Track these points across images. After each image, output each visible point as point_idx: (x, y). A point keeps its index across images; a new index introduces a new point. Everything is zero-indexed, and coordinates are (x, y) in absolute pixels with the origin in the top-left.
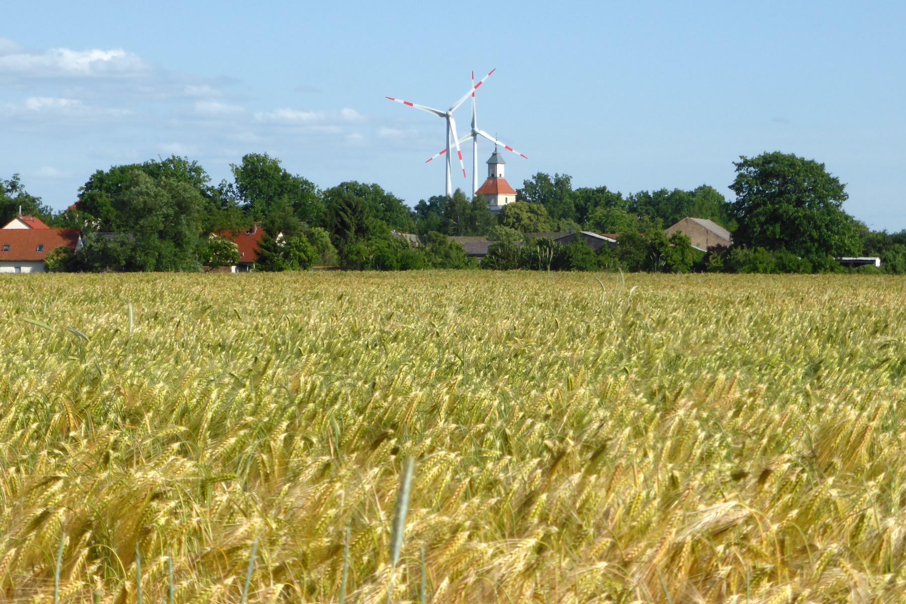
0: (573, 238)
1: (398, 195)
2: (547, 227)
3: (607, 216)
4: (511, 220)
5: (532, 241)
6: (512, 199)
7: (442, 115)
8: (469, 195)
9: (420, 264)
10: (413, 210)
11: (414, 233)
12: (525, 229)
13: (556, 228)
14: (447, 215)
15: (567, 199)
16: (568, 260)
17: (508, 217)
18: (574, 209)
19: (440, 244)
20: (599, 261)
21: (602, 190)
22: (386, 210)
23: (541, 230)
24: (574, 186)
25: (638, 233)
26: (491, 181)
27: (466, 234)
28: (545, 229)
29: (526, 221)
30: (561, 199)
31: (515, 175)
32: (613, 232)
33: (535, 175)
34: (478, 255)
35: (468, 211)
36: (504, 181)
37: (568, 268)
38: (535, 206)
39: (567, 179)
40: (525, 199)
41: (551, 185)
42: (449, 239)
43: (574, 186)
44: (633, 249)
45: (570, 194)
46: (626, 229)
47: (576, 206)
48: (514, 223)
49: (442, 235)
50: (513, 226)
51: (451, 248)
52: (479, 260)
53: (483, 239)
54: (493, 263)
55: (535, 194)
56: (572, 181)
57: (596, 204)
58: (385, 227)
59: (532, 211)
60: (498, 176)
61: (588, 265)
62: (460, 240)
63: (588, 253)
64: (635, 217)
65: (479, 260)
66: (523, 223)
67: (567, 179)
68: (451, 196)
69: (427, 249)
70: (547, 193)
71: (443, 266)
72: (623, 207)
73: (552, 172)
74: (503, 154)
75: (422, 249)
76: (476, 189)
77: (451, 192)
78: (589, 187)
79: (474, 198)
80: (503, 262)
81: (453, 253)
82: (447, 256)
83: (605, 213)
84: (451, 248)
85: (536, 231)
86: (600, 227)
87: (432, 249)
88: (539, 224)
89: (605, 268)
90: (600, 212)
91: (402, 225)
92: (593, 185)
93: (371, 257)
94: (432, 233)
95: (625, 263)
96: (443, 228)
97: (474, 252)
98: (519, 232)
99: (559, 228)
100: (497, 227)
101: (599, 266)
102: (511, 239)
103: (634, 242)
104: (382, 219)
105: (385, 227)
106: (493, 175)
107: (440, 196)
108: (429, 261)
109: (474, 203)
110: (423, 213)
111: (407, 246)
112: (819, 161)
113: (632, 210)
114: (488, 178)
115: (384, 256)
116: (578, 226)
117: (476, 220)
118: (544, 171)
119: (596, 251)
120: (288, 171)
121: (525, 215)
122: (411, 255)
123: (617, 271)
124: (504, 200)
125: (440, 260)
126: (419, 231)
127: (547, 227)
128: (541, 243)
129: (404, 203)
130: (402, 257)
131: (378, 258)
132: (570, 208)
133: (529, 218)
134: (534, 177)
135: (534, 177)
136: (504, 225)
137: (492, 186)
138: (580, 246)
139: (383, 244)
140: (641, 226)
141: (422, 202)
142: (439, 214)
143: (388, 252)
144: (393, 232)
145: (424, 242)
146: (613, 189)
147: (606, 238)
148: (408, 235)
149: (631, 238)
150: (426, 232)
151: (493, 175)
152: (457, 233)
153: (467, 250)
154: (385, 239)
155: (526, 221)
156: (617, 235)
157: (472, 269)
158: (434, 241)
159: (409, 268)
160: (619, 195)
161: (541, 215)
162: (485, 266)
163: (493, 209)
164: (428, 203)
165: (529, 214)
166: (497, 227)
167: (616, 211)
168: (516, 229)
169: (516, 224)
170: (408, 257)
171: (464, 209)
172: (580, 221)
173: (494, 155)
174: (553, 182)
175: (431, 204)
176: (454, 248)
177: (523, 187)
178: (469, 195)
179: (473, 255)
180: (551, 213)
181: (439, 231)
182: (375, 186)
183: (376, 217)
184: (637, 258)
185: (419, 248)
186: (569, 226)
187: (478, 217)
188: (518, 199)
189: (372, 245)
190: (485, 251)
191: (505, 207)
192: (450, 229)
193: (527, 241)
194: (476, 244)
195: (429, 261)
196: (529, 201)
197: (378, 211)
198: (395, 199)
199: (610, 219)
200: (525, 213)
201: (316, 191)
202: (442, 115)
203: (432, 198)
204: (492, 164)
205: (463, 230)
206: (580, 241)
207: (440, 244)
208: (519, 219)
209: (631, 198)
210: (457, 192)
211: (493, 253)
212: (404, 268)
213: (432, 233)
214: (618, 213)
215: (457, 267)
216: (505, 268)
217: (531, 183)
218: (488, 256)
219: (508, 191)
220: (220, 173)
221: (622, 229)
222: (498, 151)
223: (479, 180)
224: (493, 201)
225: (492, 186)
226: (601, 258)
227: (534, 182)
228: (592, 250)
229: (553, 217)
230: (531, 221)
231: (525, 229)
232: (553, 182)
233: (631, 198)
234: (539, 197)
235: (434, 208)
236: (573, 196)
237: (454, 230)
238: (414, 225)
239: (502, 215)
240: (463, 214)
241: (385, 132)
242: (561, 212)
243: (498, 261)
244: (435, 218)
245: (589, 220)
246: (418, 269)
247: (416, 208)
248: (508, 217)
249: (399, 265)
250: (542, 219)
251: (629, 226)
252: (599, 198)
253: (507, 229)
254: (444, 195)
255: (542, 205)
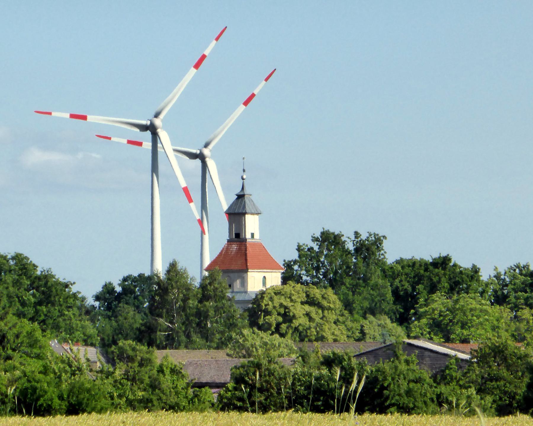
0: (390, 352)
1: (61, 274)
2: (341, 332)
3: (452, 311)
4: (273, 319)
5: (313, 359)
6: (274, 279)
7: (192, 156)
8: (195, 274)
9: (103, 402)
10: (90, 301)
11: (92, 345)
12: (302, 336)
13: (358, 334)
14: (154, 311)
15: (377, 278)
16: (380, 394)
17: (267, 313)
18: (389, 296)
19: (141, 365)
20: (439, 396)
21: (443, 262)
22: (40, 303)
23: (330, 338)
24: (391, 253)
25: (511, 343)
26: (235, 247)
27: (189, 345)
28: (338, 336)
29: (301, 321)
30: (365, 280)
31: (279, 233)
32: (465, 341)
33: (318, 235)
34: (213, 385)
35: (192, 303)
36: (260, 246)
37: (382, 410)
38: (316, 292)
39: (377, 242)
40: (298, 280)
41: (348, 252)
42: (159, 356)
43: (391, 253)
44: (504, 373)
45: (383, 271)
46: (490, 335)
47: (395, 292)
48: (278, 325)
49: (144, 348)
50: (277, 330)
51: (161, 370)
52: (212, 395)
53: (221, 355)
54: (241, 399)
55: (317, 269)
56: (385, 244)
57: (433, 289)
58: (38, 334)
59: (311, 301)
60: (248, 236)
61: (420, 404)
62: (175, 357)
63: (417, 381)
64: (505, 313)
65: (212, 395)
66: (296, 323)
67: (377, 242)
68: (162, 275)
69: (118, 373)
70: (341, 266)
71: (146, 404)
72: (482, 293)
73: (349, 228)
74: (255, 196)
75: (109, 374)
76: (207, 262)
77: (160, 269)
78: (418, 257)
79: (204, 279)
80: (259, 398)
81: (166, 381)
82: (154, 386)
83: (450, 303)
84: (161, 370)
85: (321, 338)
86: (441, 329)
87: (127, 373)
88: (326, 327)
89: (450, 409)
90: (439, 302)
91: (71, 330)
92: (427, 253)
93: (10, 391)
94: (126, 344)
95: (489, 399)
96: (146, 335)
97: (204, 380)
98: (288, 341)
99: (362, 332)
100: (246, 332)
101: (441, 402)
102: (273, 353)
103: (505, 359)
104: (32, 320)
105: (38, 334)
106: (238, 235)
107: (141, 276)
108: (120, 396)
109: (203, 287)
110: (109, 308)
111: (79, 369)
112: (143, 273)
113: (500, 299)
114: (230, 241)
115: (34, 389)
116: (400, 330)
117: (206, 317)
118: (335, 229)
119: (434, 377)
120: (459, 263)
121: (299, 310)
122: (88, 386)
123: (472, 413)
124: (259, 281)
125: (140, 394)
126: (103, 339)
127: (341, 332)
128: (329, 362)
129: (74, 289)
130: (71, 391)
131: (24, 392)
132: (383, 296)
133: (308, 315)
134: (315, 239)
135: (315, 239)
136: (260, 328)
137: (237, 255)
138: (403, 367)
139: (33, 366)
140: (517, 329)
141: (108, 289)
142: (138, 308)
143: (45, 384)
144: (54, 343)
145: (111, 361)
146: (463, 260)
147: (452, 353)
148: (82, 349)
149: (499, 352)
150: (115, 343)
151: (238, 235)
152: (171, 342)
153: (192, 374)
154: (38, 357)
155: (301, 321)
156: (474, 345)
157: (202, 411)
158: (130, 359)
159: (83, 411)
160: (476, 270)
161: (329, 309)
162: (226, 405)
163: (238, 297)
164: (118, 289)
165: (307, 308)
166: (246, 332)
167: (470, 301)
168: (282, 335)
169: (284, 326)
170: (81, 389)
171: (185, 300)
172: (403, 320)
173: (241, 197)
174: (350, 246)
175: (123, 289)
176: (167, 371)
177: (295, 256)
178: (195, 274)
179: (201, 385)
180: (348, 305)
181: (139, 339)
182: (18, 258)
183: (20, 315)
184: (510, 388)
185: (101, 372)
186: (382, 329)
187: (211, 313)
188: (285, 280)
189: (14, 368)
190: (226, 377)
191: (262, 294)
192: (161, 335)
193: (304, 358)
194: (209, 364)
195: (120, 396)
196: (306, 283)
197: (23, 304)
198: (58, 283)
199: (459, 316)
200: (299, 306)
201: (29, 261)
202: (192, 156)
203: (125, 280)
204: (236, 214)
205: (183, 338)
206: (403, 358)
207: (141, 365)
208: (287, 317)
209: (498, 277)
210: (172, 268)
211: (239, 380)
212: (74, 409)
213: (126, 344)
214: (474, 304)
215: (174, 408)
216: (264, 409)
217: (311, 249)
218: (231, 385)
219: (268, 264)
220: (419, 259)
221: (482, 337)
222: (247, 191)
223: (214, 243)
224: (237, 284)
225: (237, 255)
226: (443, 389)
227: (316, 248)
228: (426, 375)
229: (351, 312)
230: (311, 319)
231: (302, 336)
232: (350, 246)
233: (498, 277)
234: (325, 275)
235: (130, 298)
236: (390, 273)
237: (168, 337)
238: (91, 330)
239: (256, 312)
240: (183, 309)
241: (36, 157)
242: (366, 304)
243: (250, 396)
244: (132, 317)
245: (419, 319)
246: (101, 411)
247: (97, 298)
248: (267, 313)
249: (64, 405)
250: (332, 317)
251: (494, 328)
252: (441, 275)
253: (266, 336)
254: (147, 273)
255: (330, 292)
